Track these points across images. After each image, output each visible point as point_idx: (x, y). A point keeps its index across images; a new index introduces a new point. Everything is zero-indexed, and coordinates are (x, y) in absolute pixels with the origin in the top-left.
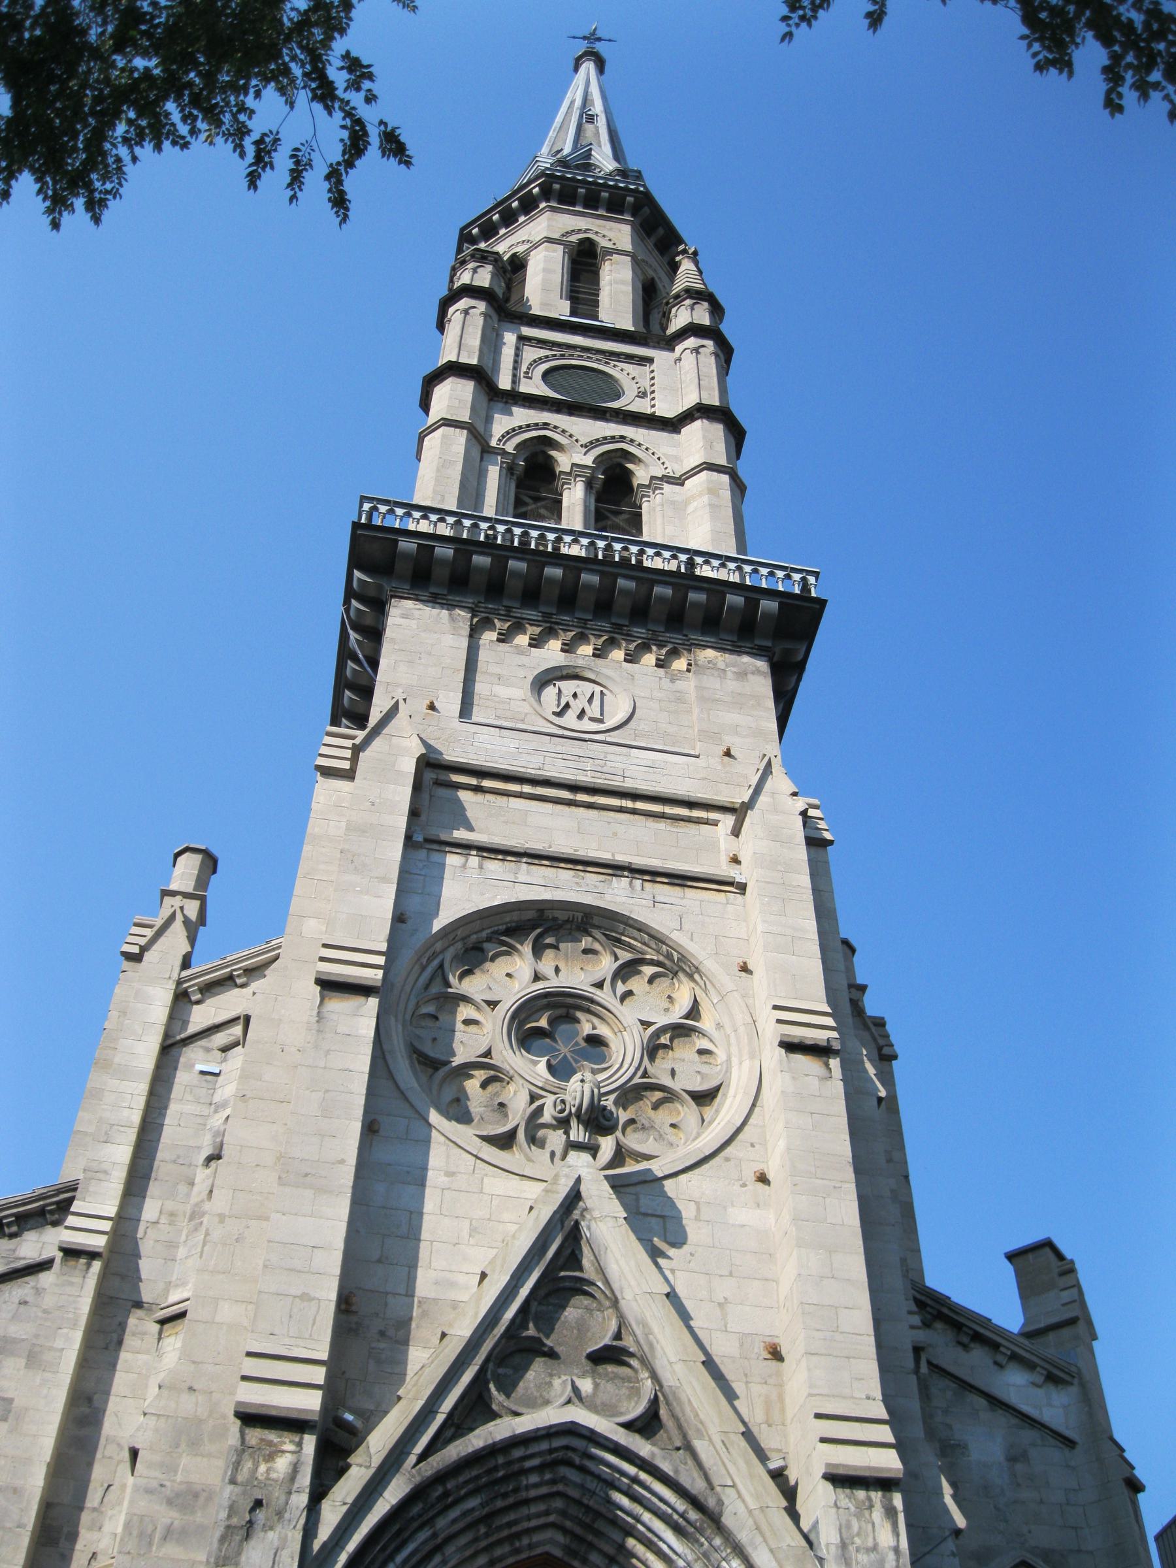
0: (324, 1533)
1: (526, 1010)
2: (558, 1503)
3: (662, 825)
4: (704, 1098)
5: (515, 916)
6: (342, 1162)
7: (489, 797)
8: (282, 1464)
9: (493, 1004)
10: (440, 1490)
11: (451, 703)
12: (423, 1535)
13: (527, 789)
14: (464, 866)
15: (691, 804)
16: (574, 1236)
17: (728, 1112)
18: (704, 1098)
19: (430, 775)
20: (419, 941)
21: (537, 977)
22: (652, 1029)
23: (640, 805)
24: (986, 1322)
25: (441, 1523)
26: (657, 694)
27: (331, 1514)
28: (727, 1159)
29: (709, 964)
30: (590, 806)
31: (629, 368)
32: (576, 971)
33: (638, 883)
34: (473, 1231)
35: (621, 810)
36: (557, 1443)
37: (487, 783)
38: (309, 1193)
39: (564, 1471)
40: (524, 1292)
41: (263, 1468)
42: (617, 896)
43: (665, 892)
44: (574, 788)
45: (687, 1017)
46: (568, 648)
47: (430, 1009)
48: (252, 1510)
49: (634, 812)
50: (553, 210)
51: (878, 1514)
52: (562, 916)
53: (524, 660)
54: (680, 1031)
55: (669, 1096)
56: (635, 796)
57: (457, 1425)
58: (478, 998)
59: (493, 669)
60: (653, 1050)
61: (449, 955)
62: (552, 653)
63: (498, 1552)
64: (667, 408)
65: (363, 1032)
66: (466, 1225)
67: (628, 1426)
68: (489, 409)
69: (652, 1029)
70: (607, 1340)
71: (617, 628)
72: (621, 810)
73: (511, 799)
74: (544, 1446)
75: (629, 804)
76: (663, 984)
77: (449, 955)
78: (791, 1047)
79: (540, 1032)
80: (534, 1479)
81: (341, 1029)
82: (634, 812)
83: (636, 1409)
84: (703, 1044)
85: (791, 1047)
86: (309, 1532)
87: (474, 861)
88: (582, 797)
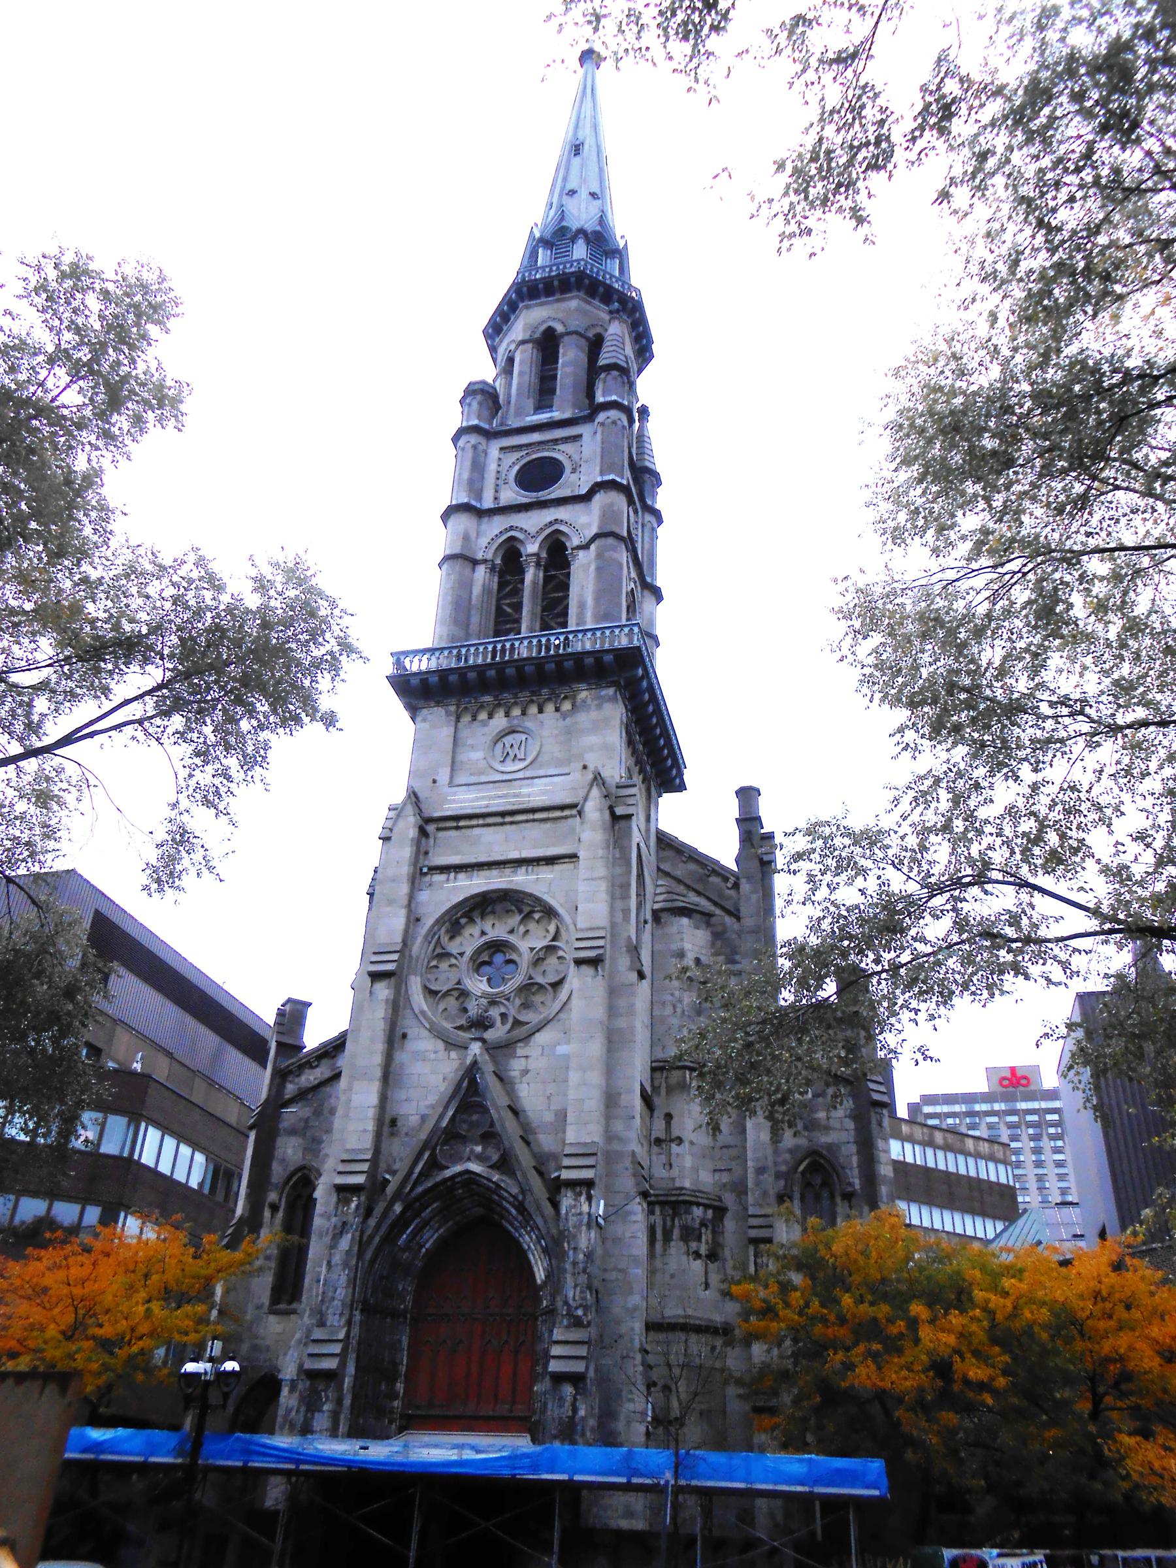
0: (369, 1232)
1: (479, 951)
3: (548, 825)
9: (462, 954)
11: (444, 776)
13: (481, 822)
16: (473, 1082)
17: (563, 995)
18: (557, 985)
19: (431, 828)
20: (423, 929)
21: (483, 933)
23: (538, 816)
24: (717, 862)
27: (372, 1222)
29: (560, 910)
30: (512, 823)
31: (562, 447)
32: (496, 929)
35: (527, 821)
37: (462, 823)
40: (450, 1113)
42: (520, 880)
43: (546, 874)
44: (503, 814)
45: (554, 940)
46: (507, 715)
47: (434, 963)
49: (489, 825)
50: (527, 307)
51: (583, 1198)
52: (494, 895)
53: (486, 730)
55: (541, 987)
56: (533, 811)
57: (424, 1175)
58: (454, 952)
59: (469, 742)
60: (537, 962)
61: (443, 929)
62: (500, 721)
64: (583, 491)
68: (479, 525)
70: (486, 1129)
71: (534, 693)
72: (527, 821)
75: (531, 816)
76: (545, 922)
77: (443, 929)
78: (579, 962)
79: (484, 963)
83: (495, 1157)
84: (561, 953)
85: (579, 962)
86: (362, 1233)
88: (508, 819)
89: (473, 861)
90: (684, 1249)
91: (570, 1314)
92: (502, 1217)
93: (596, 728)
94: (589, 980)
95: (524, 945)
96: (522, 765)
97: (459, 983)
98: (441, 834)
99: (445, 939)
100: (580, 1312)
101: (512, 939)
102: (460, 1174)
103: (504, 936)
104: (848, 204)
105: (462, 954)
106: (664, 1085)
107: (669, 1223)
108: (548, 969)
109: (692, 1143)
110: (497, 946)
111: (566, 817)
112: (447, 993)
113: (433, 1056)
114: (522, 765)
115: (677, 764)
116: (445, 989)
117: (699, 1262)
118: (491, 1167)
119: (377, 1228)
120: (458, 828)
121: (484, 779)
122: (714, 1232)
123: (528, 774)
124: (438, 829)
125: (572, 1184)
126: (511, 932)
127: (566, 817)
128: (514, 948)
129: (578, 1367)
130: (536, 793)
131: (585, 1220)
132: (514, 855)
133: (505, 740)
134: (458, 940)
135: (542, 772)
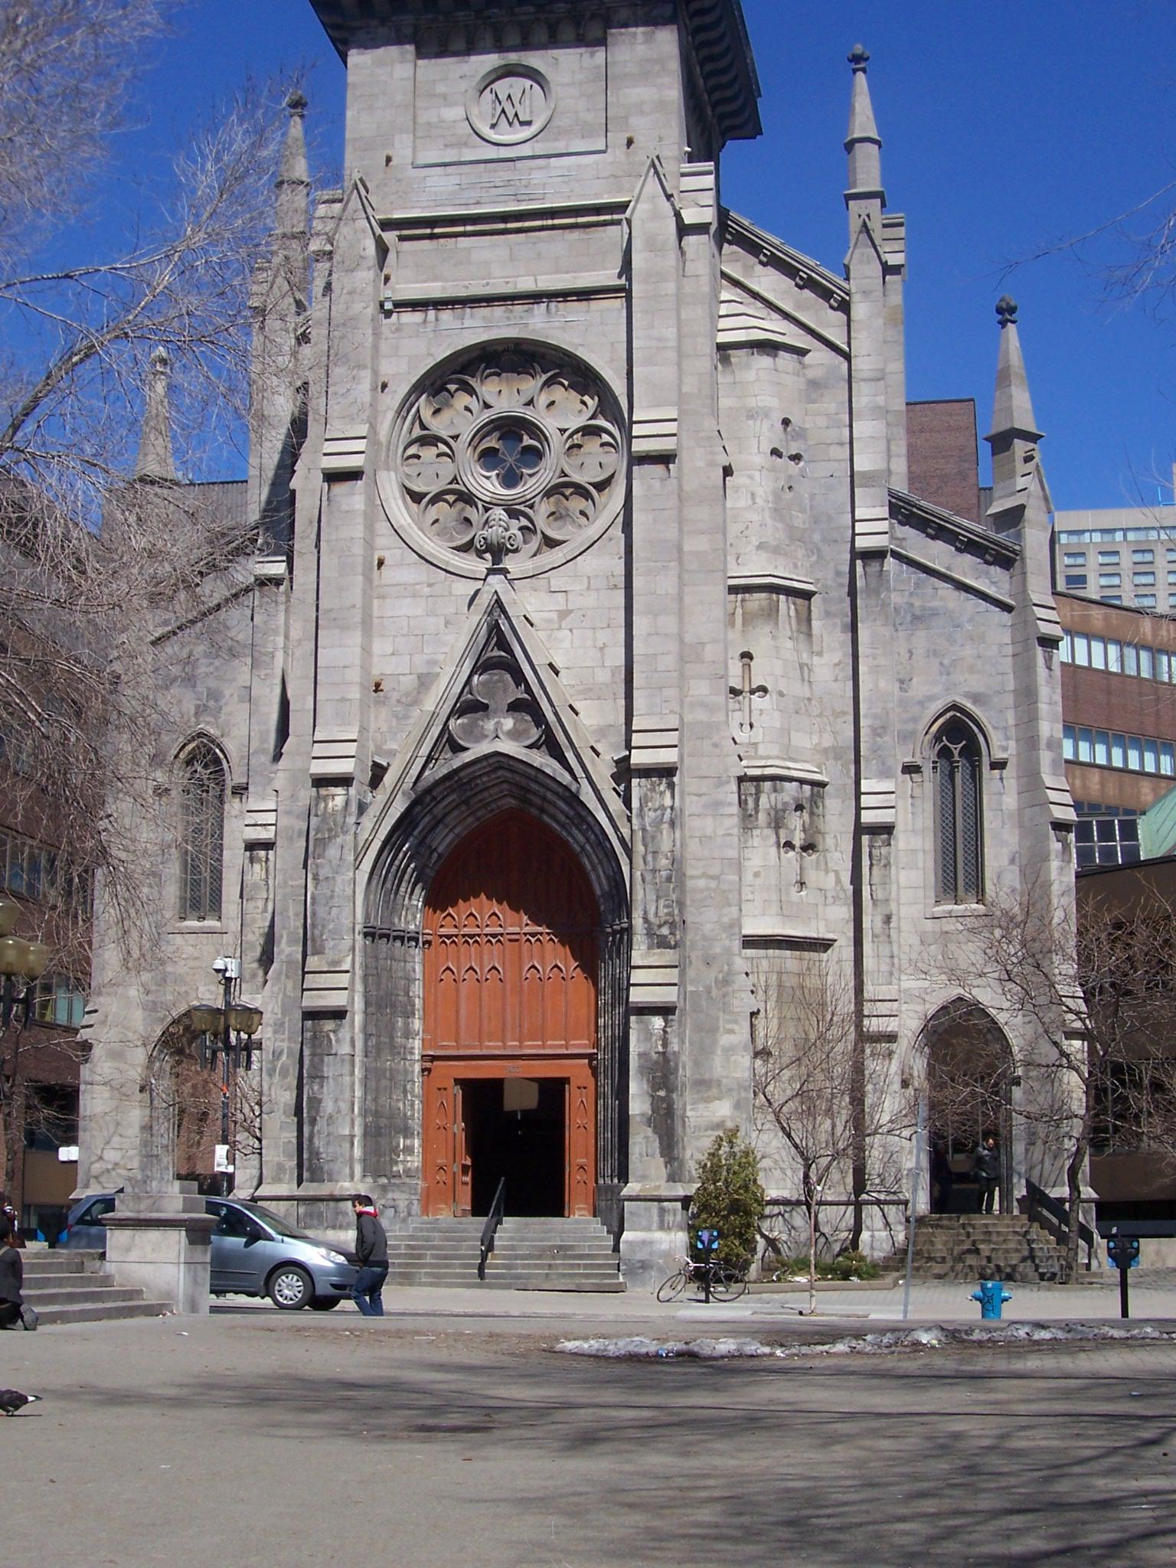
2: (505, 786)
3: (576, 235)
4: (551, 543)
5: (466, 357)
6: (354, 606)
7: (442, 241)
8: (339, 801)
10: (429, 798)
12: (426, 820)
14: (425, 321)
15: (597, 210)
18: (551, 543)
22: (567, 434)
25: (435, 811)
26: (579, 77)
28: (610, 540)
32: (503, 395)
33: (553, 305)
34: (447, 623)
36: (491, 761)
38: (337, 631)
39: (500, 773)
41: (330, 805)
43: (574, 310)
47: (412, 451)
48: (780, 456)
49: (553, 228)
54: (581, 491)
56: (553, 213)
58: (444, 434)
63: (479, 814)
65: (357, 506)
66: (442, 621)
67: (529, 747)
69: (567, 434)
73: (460, 239)
74: (485, 763)
80: (485, 779)
81: (344, 507)
82: (553, 228)
87: (432, 314)
89: (463, 293)
90: (773, 838)
91: (650, 934)
92: (542, 810)
93: (644, 76)
94: (657, 484)
95: (550, 423)
96: (527, 132)
97: (455, 480)
98: (407, 246)
99: (426, 414)
100: (665, 931)
101: (529, 414)
102: (486, 757)
103: (519, 411)
104: (928, 1006)
105: (455, 437)
106: (739, 611)
107: (751, 804)
108: (588, 461)
109: (781, 694)
110: (511, 428)
111: (605, 224)
112: (437, 498)
113: (427, 590)
114: (527, 132)
115: (750, 92)
116: (434, 489)
117: (791, 854)
118: (529, 747)
119: (375, 830)
120: (432, 237)
121: (468, 155)
122: (812, 814)
123: (539, 148)
124: (402, 238)
125: (647, 772)
126: (530, 403)
127: (605, 224)
128: (534, 430)
129: (668, 995)
130: (552, 186)
131: (667, 817)
132: (526, 285)
133: (496, 86)
134: (446, 415)
135: (560, 146)
